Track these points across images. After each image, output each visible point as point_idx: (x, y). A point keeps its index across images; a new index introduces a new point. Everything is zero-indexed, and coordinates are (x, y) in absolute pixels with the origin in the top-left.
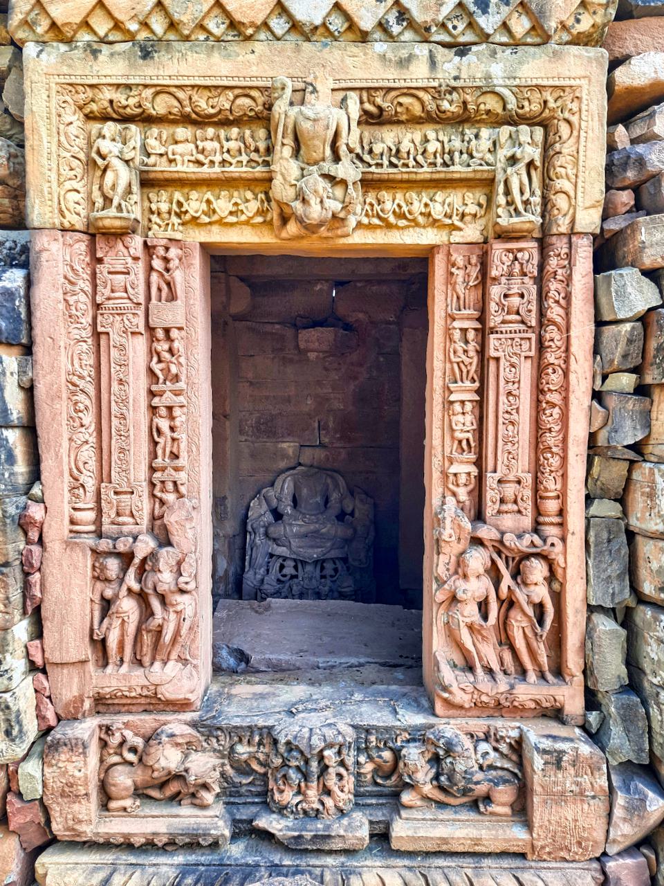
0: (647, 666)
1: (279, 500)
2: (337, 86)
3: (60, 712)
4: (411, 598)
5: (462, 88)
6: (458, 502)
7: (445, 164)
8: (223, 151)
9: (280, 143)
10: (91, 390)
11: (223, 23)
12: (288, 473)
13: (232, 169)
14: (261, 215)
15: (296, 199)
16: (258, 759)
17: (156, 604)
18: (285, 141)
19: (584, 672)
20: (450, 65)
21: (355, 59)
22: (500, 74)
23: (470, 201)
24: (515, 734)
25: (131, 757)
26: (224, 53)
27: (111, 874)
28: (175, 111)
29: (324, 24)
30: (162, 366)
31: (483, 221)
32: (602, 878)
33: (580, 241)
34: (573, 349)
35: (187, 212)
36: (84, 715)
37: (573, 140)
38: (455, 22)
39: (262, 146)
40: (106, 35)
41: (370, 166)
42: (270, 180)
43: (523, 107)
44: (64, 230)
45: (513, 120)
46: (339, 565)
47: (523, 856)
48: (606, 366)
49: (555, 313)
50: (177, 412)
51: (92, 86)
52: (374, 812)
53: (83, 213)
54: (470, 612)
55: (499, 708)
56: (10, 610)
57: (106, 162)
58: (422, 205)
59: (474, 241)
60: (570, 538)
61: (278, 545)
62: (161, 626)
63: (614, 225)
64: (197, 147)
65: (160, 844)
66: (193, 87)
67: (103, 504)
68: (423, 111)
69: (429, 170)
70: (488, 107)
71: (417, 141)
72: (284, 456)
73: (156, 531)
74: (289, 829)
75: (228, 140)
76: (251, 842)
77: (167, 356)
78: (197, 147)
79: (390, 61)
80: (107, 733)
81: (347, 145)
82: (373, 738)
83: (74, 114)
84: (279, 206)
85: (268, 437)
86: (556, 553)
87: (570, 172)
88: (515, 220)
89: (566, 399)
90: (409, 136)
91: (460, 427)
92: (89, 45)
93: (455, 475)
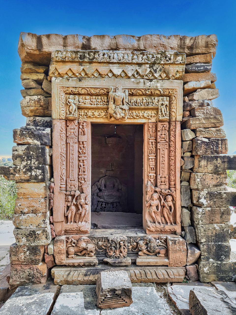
0: (195, 220)
1: (101, 186)
3: (56, 234)
4: (140, 211)
6: (151, 182)
7: (147, 105)
8: (98, 102)
10: (65, 157)
12: (103, 178)
13: (99, 106)
16: (104, 245)
17: (80, 207)
18: (112, 100)
19: (181, 222)
20: (148, 84)
22: (159, 86)
23: (153, 113)
24: (165, 237)
25: (74, 245)
27: (70, 272)
28: (86, 93)
29: (120, 75)
30: (81, 150)
31: (156, 117)
32: (186, 270)
33: (178, 123)
34: (176, 147)
36: (62, 235)
38: (149, 75)
39: (106, 101)
44: (60, 119)
46: (118, 204)
47: (167, 266)
48: (184, 151)
49: (172, 139)
50: (85, 161)
52: (132, 257)
53: (65, 115)
54: (154, 208)
55: (161, 232)
56: (47, 208)
57: (70, 104)
60: (177, 190)
61: (100, 198)
62: (81, 213)
63: (185, 119)
64: (91, 101)
65: (81, 265)
66: (91, 88)
67: (67, 183)
69: (144, 106)
70: (157, 93)
71: (141, 100)
72: (102, 173)
73: (79, 190)
74: (112, 261)
76: (103, 265)
77: (83, 148)
78: (91, 101)
80: (68, 239)
82: (131, 240)
85: (97, 168)
86: (174, 194)
87: (175, 108)
88: (163, 118)
89: (175, 158)
91: (151, 165)
92: (67, 78)
93: (150, 176)
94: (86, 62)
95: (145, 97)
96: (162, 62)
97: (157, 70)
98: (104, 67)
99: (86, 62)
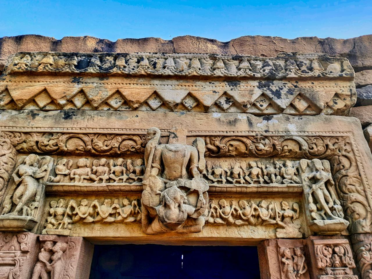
2: (190, 134)
5: (272, 137)
7: (265, 182)
8: (110, 173)
9: (150, 166)
11: (120, 102)
13: (115, 184)
14: (133, 216)
15: (160, 204)
18: (154, 165)
20: (260, 125)
21: (201, 120)
22: (295, 129)
23: (288, 208)
26: (118, 116)
28: (80, 148)
35: (77, 214)
37: (353, 168)
38: (261, 103)
39: (138, 169)
40: (45, 106)
41: (213, 182)
42: (141, 191)
43: (312, 148)
45: (310, 156)
51: (26, 133)
57: (20, 180)
58: (253, 210)
59: (295, 236)
64: (92, 170)
68: (247, 150)
70: (290, 148)
75: (115, 166)
78: (92, 170)
79: (223, 122)
81: (198, 168)
83: (9, 149)
84: (145, 207)
87: (359, 188)
88: (328, 222)
90: (238, 165)
92: (32, 111)
94: (92, 75)
95: (256, 162)
96: (292, 75)
97: (281, 91)
98: (139, 86)
99: (92, 75)
